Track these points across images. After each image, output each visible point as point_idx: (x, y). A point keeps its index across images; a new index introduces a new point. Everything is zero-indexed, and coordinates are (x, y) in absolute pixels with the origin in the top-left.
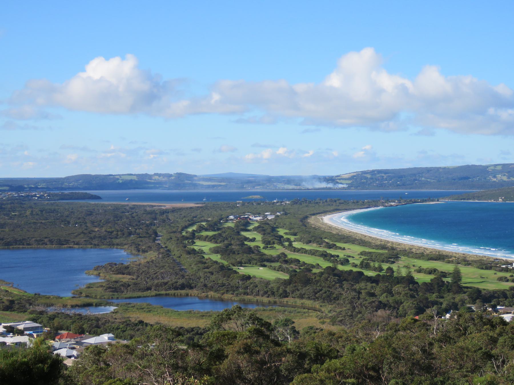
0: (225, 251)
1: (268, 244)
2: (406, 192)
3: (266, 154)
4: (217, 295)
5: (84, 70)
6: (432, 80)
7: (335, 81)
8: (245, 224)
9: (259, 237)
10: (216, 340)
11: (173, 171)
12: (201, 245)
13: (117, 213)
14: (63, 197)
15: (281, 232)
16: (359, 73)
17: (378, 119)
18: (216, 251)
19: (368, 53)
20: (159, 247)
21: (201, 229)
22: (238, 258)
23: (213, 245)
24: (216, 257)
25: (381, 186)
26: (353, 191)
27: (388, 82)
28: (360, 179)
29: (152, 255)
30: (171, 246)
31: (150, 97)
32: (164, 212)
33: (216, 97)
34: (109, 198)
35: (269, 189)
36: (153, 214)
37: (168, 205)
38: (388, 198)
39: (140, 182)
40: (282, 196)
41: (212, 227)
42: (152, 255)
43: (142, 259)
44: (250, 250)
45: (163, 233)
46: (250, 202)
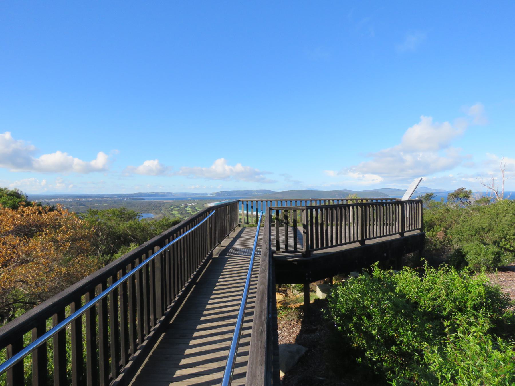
0: (181, 214)
1: (193, 211)
2: (231, 197)
3: (193, 187)
4: (89, 199)
5: (143, 164)
6: (239, 167)
7: (213, 167)
8: (187, 206)
9: (190, 210)
10: (395, 316)
11: (166, 192)
12: (174, 212)
13: (150, 204)
14: (133, 199)
15: (197, 208)
16: (220, 165)
17: (225, 178)
18: (179, 214)
19: (223, 159)
20: (162, 213)
21: (174, 208)
22: (185, 215)
23: (177, 212)
24: (179, 215)
25: (224, 196)
26: (216, 197)
27: (227, 168)
28: (218, 194)
29: (160, 215)
30: (166, 213)
31: (162, 171)
32: (163, 203)
33: (181, 172)
34: (147, 200)
35: (193, 196)
36: (161, 204)
37: (164, 201)
38: (226, 199)
39: (157, 194)
40: (197, 199)
41: (178, 207)
42: (160, 215)
43: (157, 216)
44: (188, 213)
45: (163, 209)
46: (188, 200)
